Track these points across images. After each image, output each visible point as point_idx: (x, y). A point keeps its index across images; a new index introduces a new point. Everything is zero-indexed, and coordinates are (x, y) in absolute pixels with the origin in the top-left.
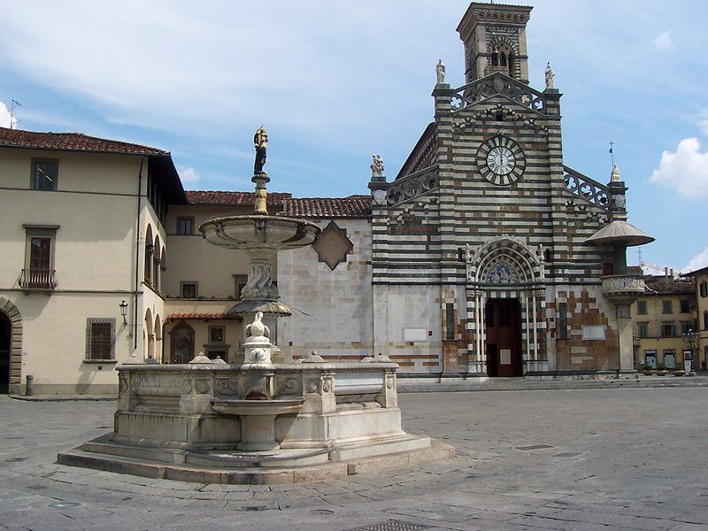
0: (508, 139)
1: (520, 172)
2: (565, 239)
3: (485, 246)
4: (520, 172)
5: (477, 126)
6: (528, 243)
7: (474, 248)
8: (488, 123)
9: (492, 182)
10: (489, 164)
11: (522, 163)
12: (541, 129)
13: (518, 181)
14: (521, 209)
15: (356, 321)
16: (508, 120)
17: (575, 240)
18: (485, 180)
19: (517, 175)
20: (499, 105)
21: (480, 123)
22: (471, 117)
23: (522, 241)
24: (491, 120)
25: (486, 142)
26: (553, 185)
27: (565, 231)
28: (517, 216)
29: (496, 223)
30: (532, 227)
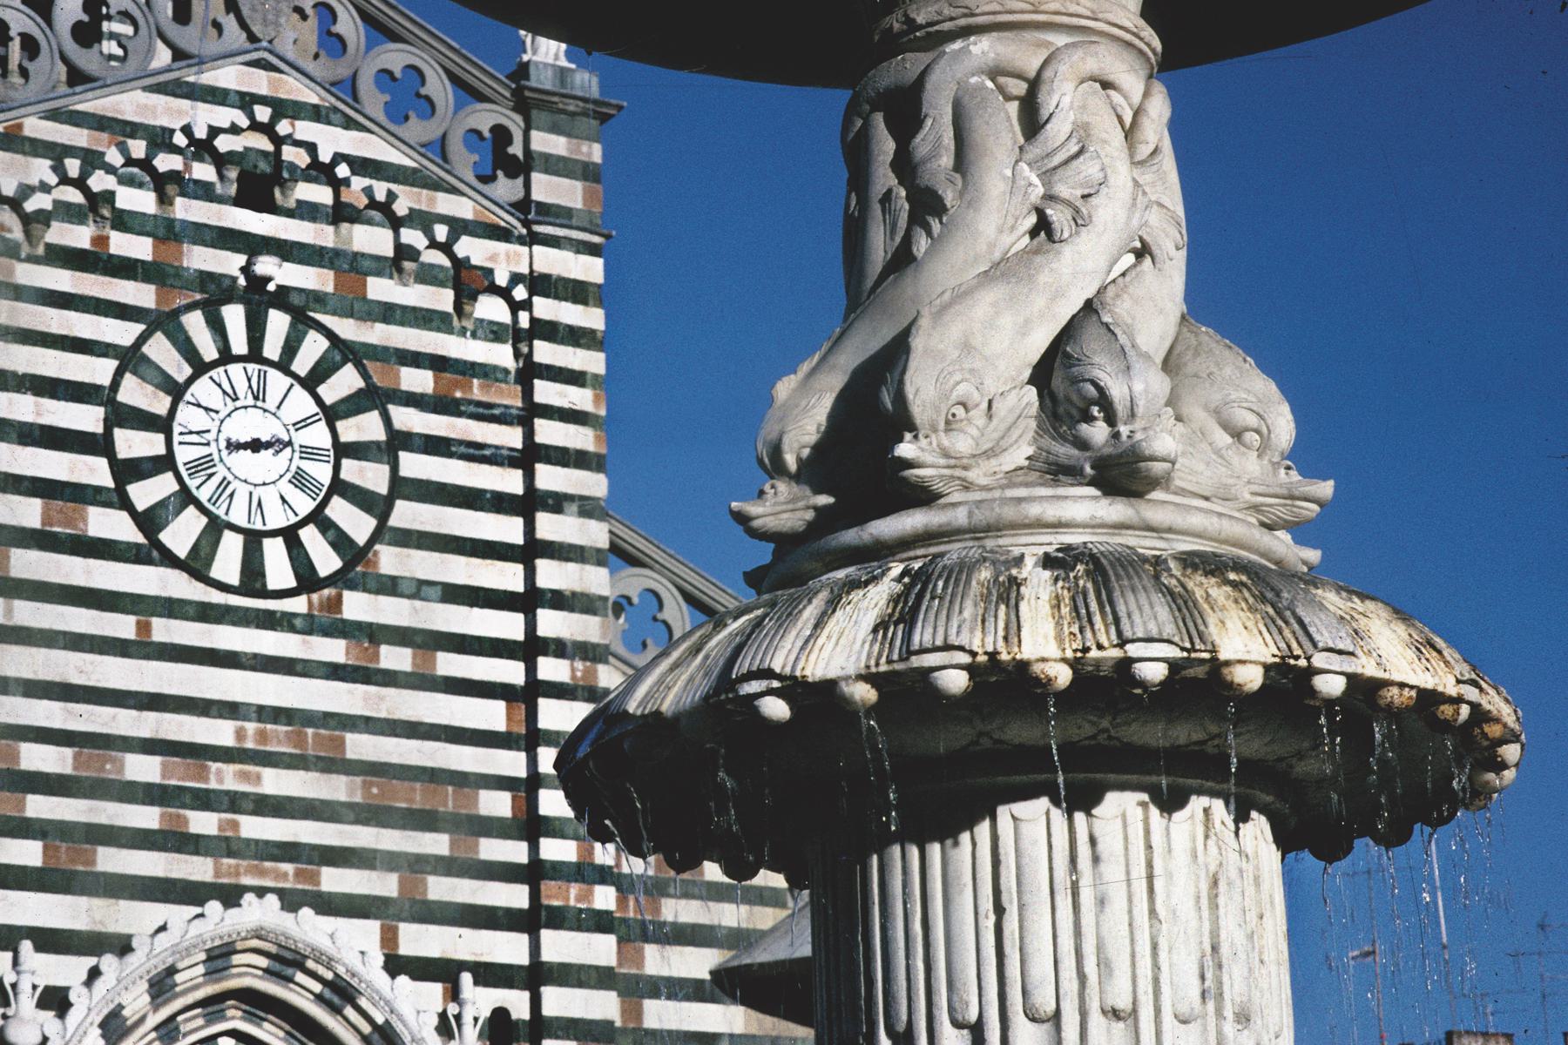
0: (302, 323)
1: (358, 525)
2: (600, 949)
3: (133, 960)
4: (358, 525)
5: (125, 221)
6: (396, 965)
7: (66, 970)
8: (186, 210)
9: (197, 565)
10: (183, 455)
11: (374, 477)
12: (494, 290)
13: (341, 579)
14: (360, 746)
15: (232, 15)
16: (307, 211)
17: (658, 961)
18: (153, 553)
19: (340, 541)
20: (263, 114)
21: (140, 200)
22: (92, 160)
23: (353, 945)
24: (205, 192)
25: (164, 322)
26: (551, 623)
27: (604, 898)
28: (336, 788)
29: (203, 823)
30: (418, 865)
